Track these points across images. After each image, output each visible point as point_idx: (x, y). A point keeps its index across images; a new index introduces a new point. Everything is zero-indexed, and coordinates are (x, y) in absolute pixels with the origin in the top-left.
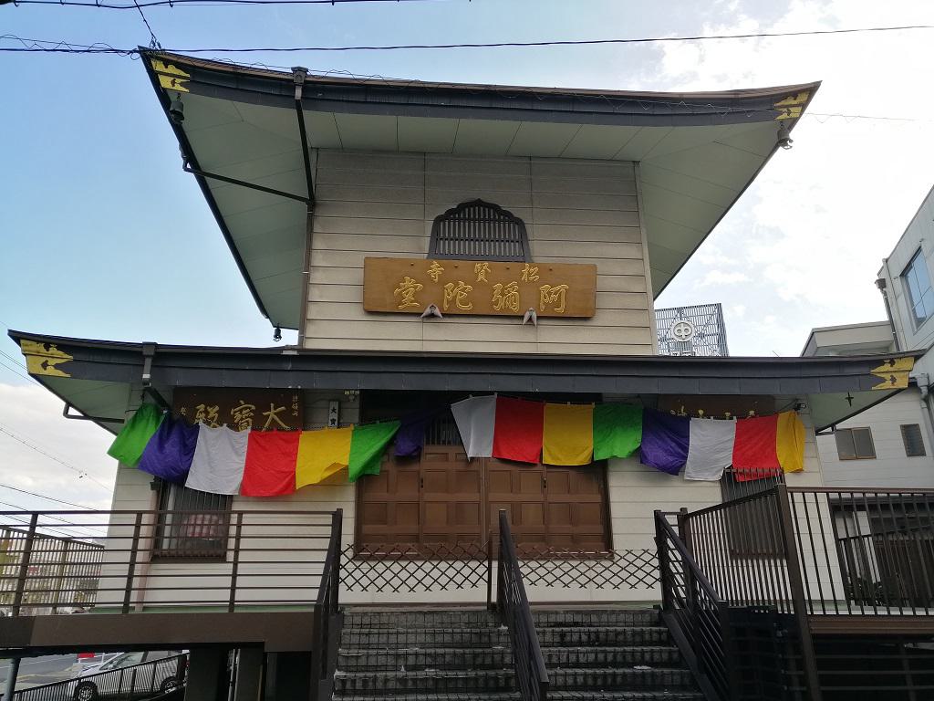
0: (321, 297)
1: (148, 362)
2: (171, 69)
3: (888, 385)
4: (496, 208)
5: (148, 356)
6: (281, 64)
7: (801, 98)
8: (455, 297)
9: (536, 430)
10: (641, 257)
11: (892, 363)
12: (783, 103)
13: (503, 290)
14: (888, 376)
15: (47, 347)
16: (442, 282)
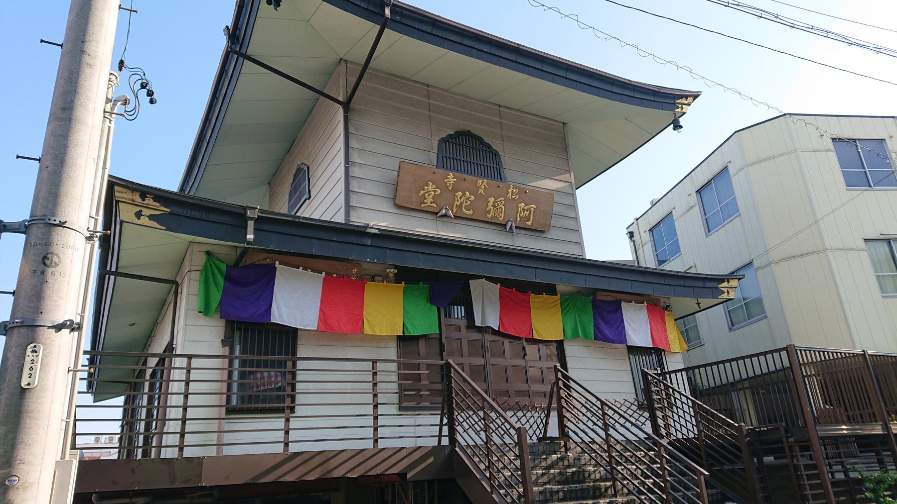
0: (359, 188)
3: (725, 296)
4: (479, 139)
5: (251, 219)
7: (690, 99)
9: (526, 308)
11: (728, 282)
12: (680, 101)
14: (725, 290)
15: (143, 196)
16: (455, 190)
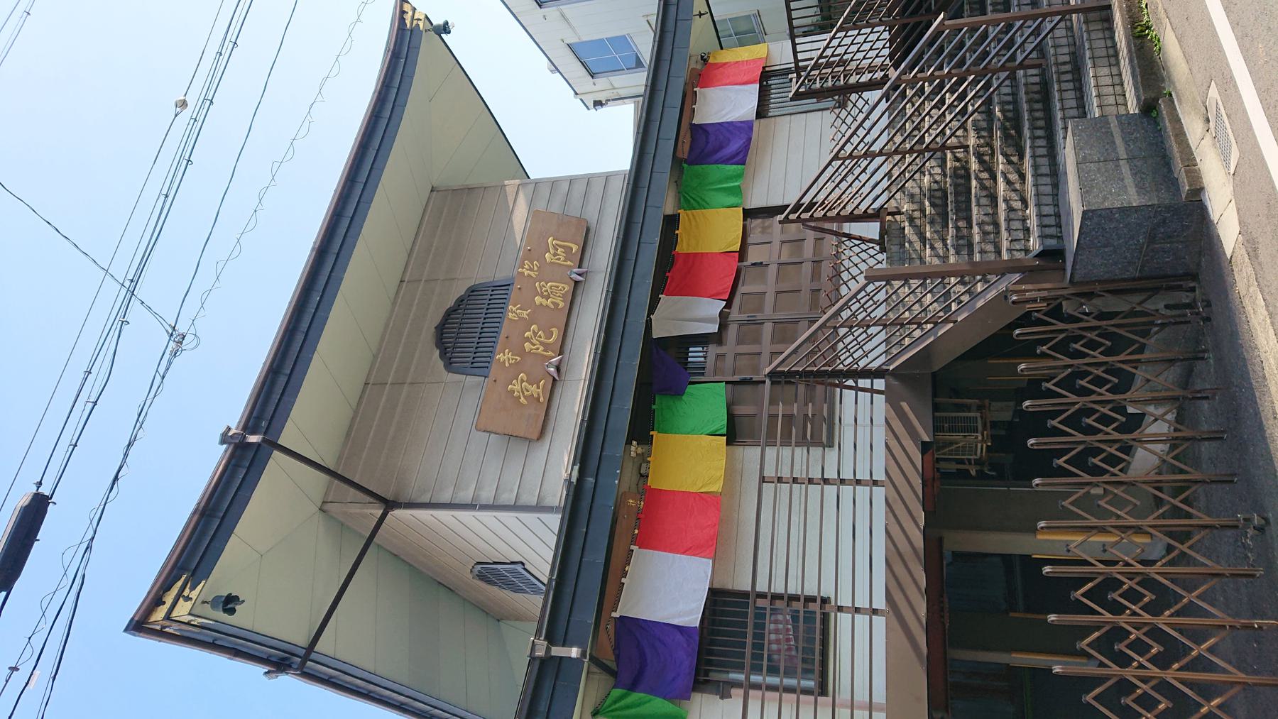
0: (512, 491)
1: (557, 651)
2: (169, 598)
4: (449, 314)
5: (548, 650)
6: (213, 457)
8: (541, 343)
9: (695, 259)
10: (534, 185)
13: (543, 297)
16: (522, 352)
